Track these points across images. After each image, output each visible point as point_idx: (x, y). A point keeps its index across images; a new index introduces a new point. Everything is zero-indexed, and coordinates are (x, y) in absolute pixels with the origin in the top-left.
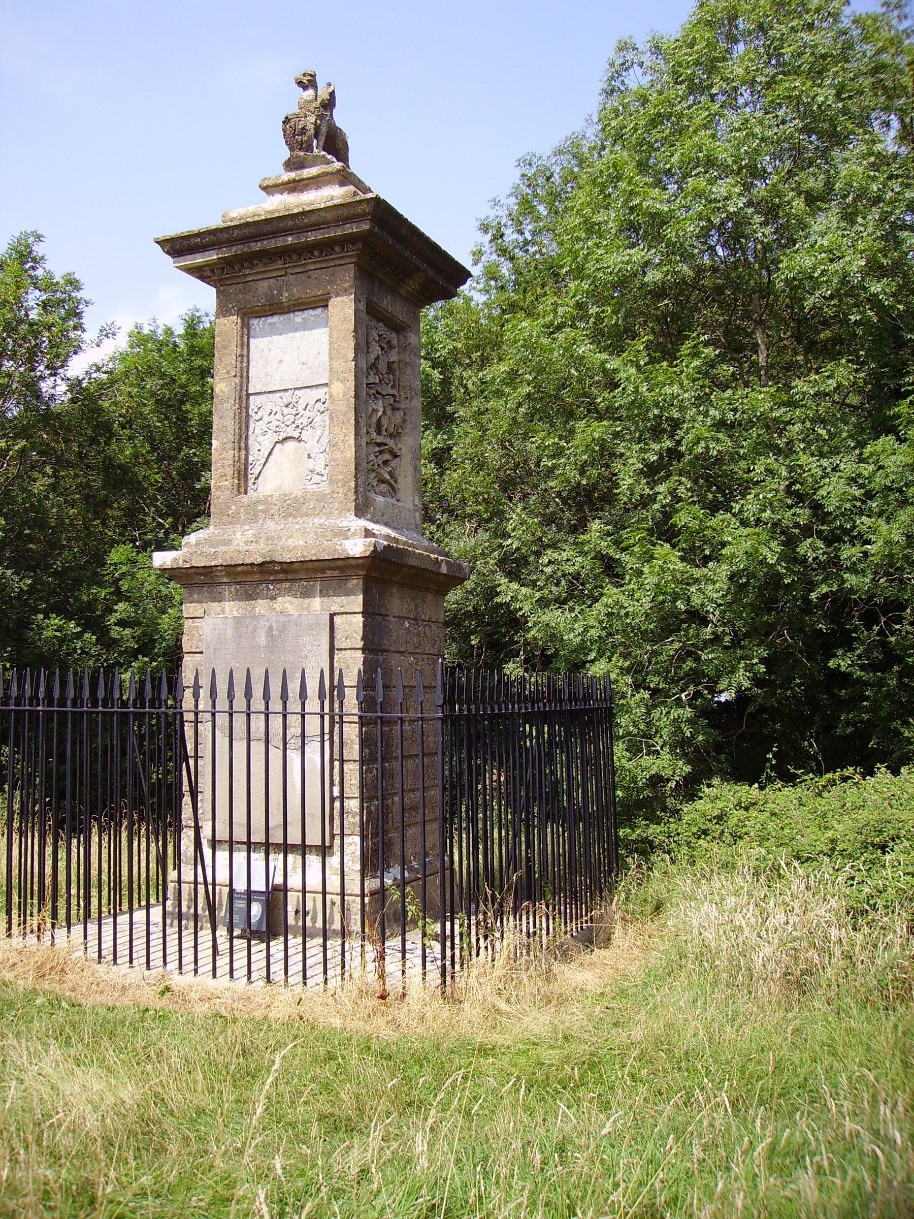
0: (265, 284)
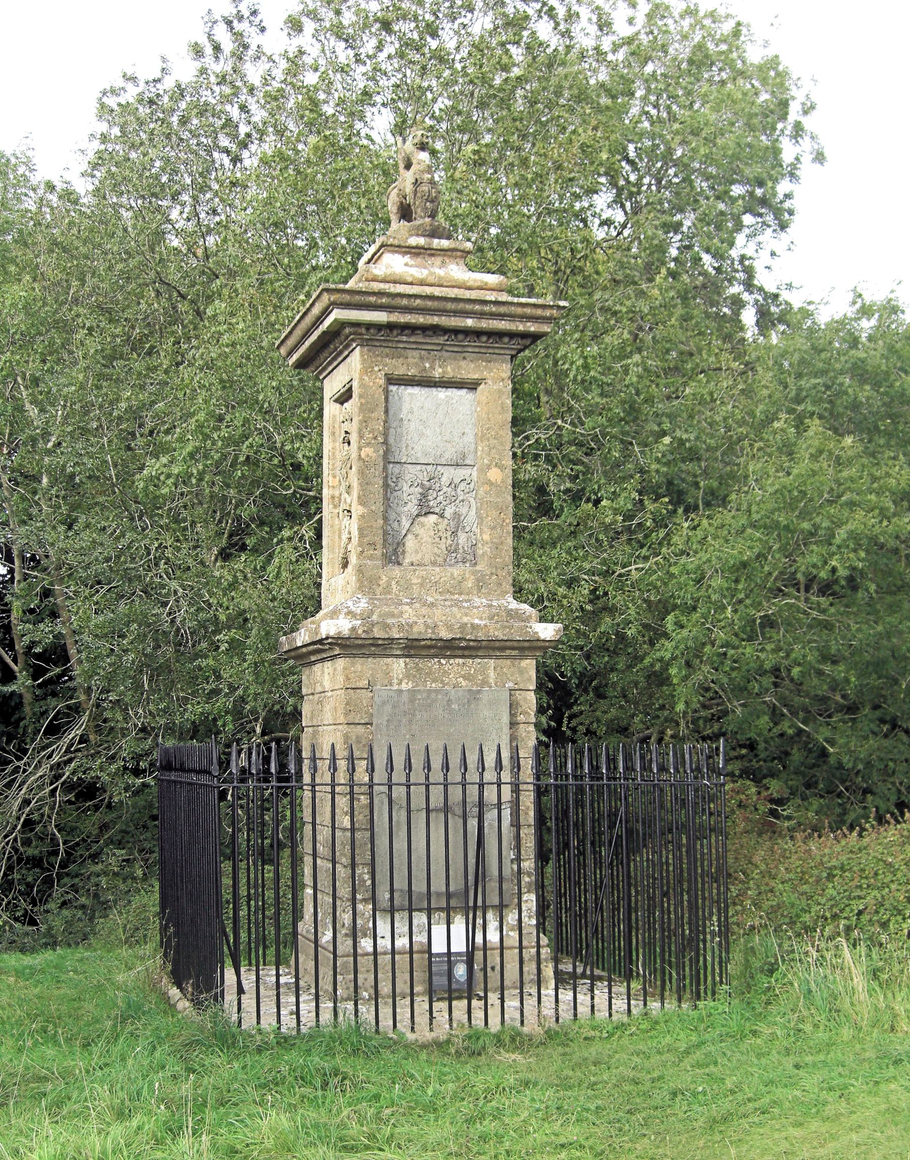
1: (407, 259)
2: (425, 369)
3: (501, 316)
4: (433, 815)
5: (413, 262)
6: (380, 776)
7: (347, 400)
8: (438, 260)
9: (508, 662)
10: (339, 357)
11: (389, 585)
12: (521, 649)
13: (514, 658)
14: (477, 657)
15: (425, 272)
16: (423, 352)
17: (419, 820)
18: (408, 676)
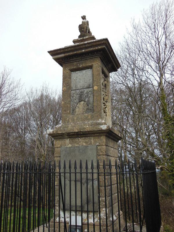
0: (76, 63)
3: (91, 47)
4: (77, 182)
6: (62, 170)
11: (69, 120)
12: (99, 133)
16: (77, 62)
17: (73, 183)
18: (70, 143)
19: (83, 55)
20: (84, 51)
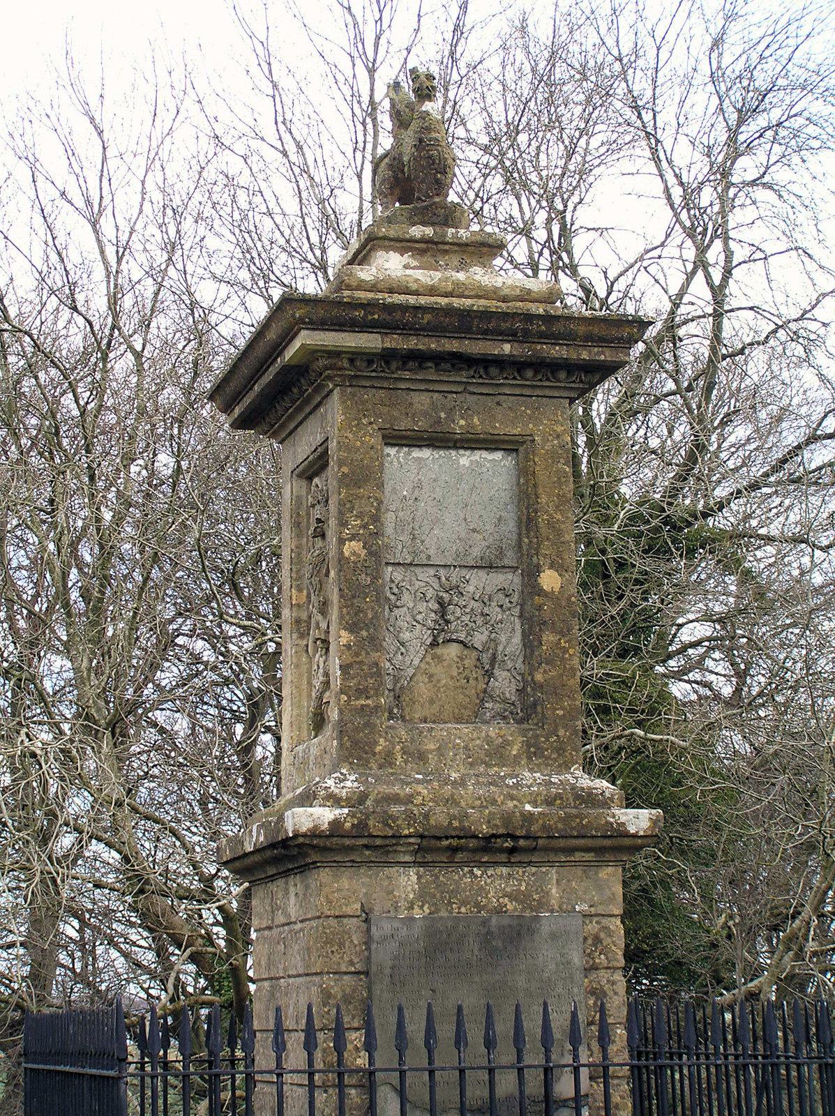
1: (406, 258)
2: (438, 421)
5: (415, 263)
7: (317, 473)
8: (455, 260)
9: (579, 871)
10: (311, 405)
13: (586, 864)
14: (530, 863)
15: (437, 275)
16: (436, 395)
19: (486, 368)
20: (511, 356)
